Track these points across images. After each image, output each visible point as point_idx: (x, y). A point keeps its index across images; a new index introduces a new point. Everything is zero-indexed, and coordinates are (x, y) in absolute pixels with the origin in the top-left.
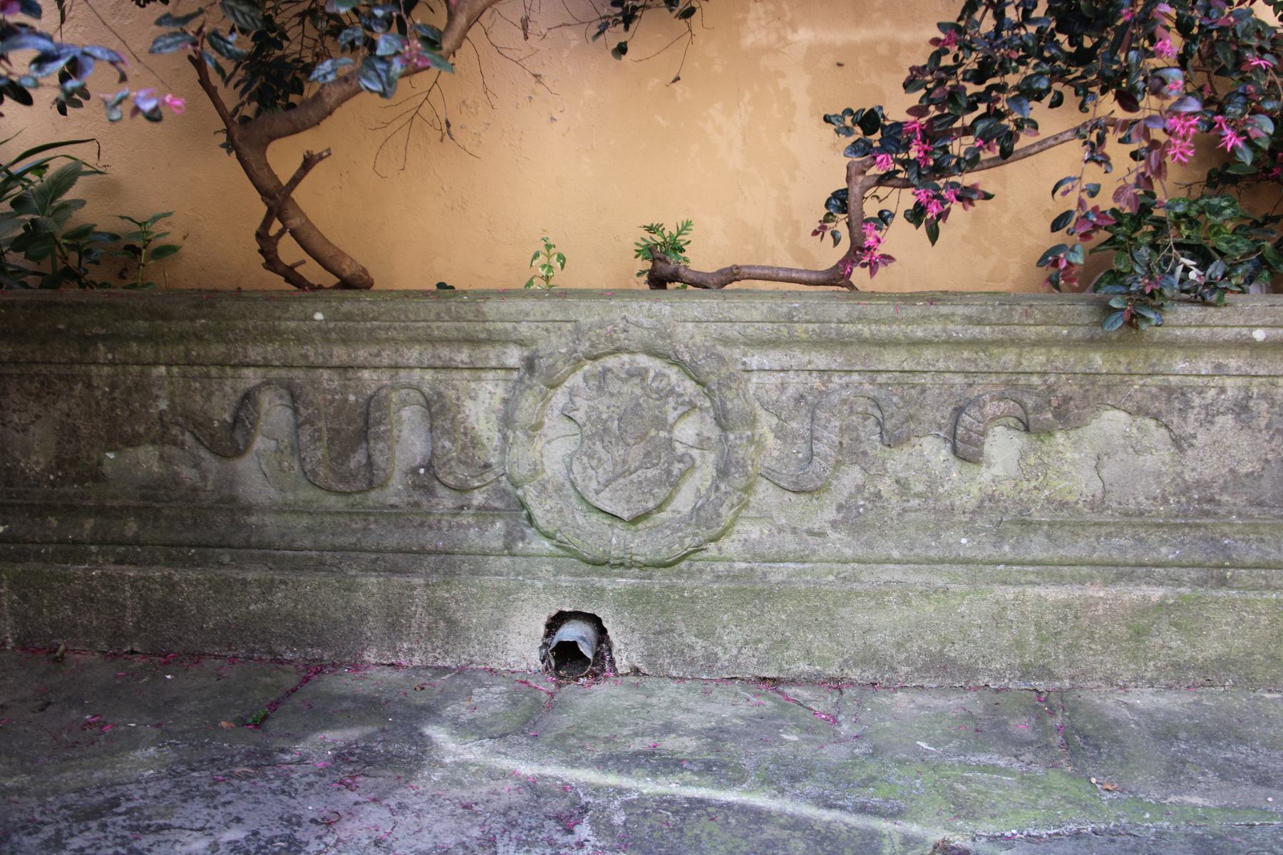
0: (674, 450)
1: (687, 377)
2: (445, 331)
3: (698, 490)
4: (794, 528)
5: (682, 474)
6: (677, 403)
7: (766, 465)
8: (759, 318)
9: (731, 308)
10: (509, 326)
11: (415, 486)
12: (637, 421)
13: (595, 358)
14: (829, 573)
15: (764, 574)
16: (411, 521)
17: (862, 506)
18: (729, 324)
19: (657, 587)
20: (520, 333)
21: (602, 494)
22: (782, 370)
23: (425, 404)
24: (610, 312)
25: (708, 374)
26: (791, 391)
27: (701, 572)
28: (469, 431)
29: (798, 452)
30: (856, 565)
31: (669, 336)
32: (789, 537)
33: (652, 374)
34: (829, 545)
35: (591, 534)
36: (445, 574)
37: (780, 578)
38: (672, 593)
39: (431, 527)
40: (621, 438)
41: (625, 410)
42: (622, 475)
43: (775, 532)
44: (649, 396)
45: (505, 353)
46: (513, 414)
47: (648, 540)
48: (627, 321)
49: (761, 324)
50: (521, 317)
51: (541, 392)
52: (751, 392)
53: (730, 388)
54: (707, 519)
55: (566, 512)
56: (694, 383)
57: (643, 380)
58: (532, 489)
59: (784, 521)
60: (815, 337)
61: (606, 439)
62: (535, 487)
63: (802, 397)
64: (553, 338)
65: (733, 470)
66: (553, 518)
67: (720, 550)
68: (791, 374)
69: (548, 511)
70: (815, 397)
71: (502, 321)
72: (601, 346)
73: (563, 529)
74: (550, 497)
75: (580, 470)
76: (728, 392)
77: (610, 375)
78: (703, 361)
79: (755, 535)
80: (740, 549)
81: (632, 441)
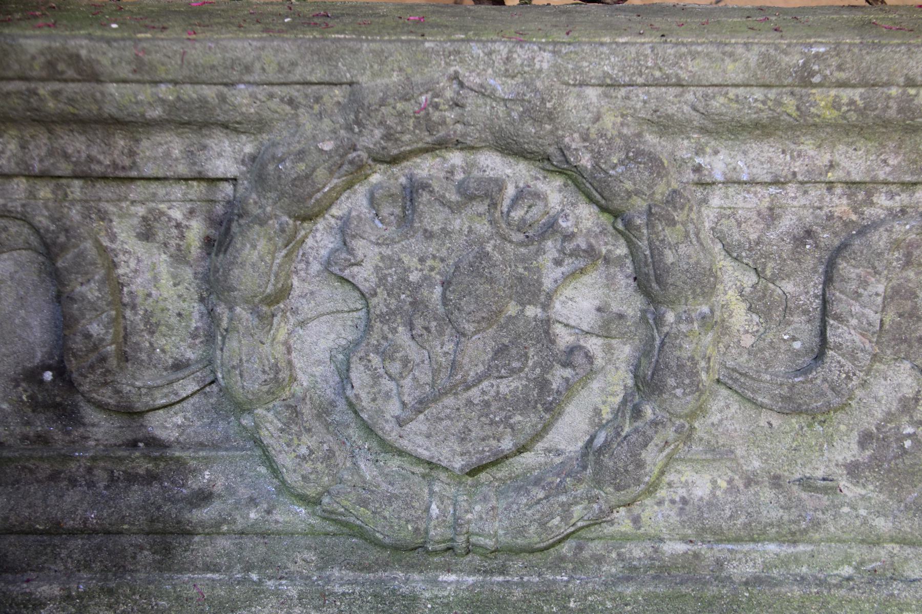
0: (553, 342)
1: (582, 197)
2: (71, 101)
3: (597, 412)
4: (777, 477)
5: (569, 387)
6: (562, 251)
7: (730, 363)
8: (739, 78)
9: (681, 56)
10: (209, 92)
11: (36, 405)
12: (482, 287)
13: (394, 160)
14: (842, 563)
15: (719, 563)
16: (31, 471)
17: (909, 436)
18: (673, 91)
19: (518, 593)
20: (235, 108)
21: (412, 426)
22: (776, 182)
23: (42, 249)
24: (426, 64)
25: (629, 194)
26: (787, 222)
27: (599, 560)
28: (139, 300)
29: (794, 339)
30: (896, 548)
31: (550, 117)
32: (767, 494)
33: (510, 191)
34: (846, 509)
35: (391, 498)
36: (105, 570)
37: (749, 570)
38: (546, 602)
39: (73, 482)
40: (448, 320)
41: (457, 267)
42: (451, 390)
43: (739, 483)
44: (504, 238)
45: (204, 147)
46: (226, 275)
47: (502, 504)
48: (461, 85)
49: (741, 91)
50: (235, 75)
51: (283, 231)
52: (707, 225)
53: (672, 223)
54: (617, 472)
55: (340, 457)
56: (594, 209)
57: (494, 205)
58: (270, 416)
59: (756, 464)
60: (853, 117)
61: (419, 322)
62: (277, 414)
63: (809, 233)
64: (305, 118)
65: (671, 382)
66: (315, 471)
67: (636, 520)
68: (792, 189)
69: (304, 458)
70: (836, 234)
71: (194, 82)
72: (406, 137)
73: (335, 488)
74: (309, 430)
75: (367, 379)
76: (667, 231)
77: (425, 197)
78: (620, 169)
79: (701, 489)
80: (674, 519)
81: (470, 327)
